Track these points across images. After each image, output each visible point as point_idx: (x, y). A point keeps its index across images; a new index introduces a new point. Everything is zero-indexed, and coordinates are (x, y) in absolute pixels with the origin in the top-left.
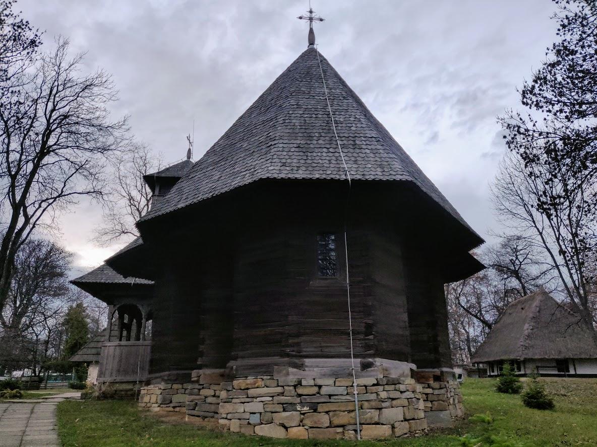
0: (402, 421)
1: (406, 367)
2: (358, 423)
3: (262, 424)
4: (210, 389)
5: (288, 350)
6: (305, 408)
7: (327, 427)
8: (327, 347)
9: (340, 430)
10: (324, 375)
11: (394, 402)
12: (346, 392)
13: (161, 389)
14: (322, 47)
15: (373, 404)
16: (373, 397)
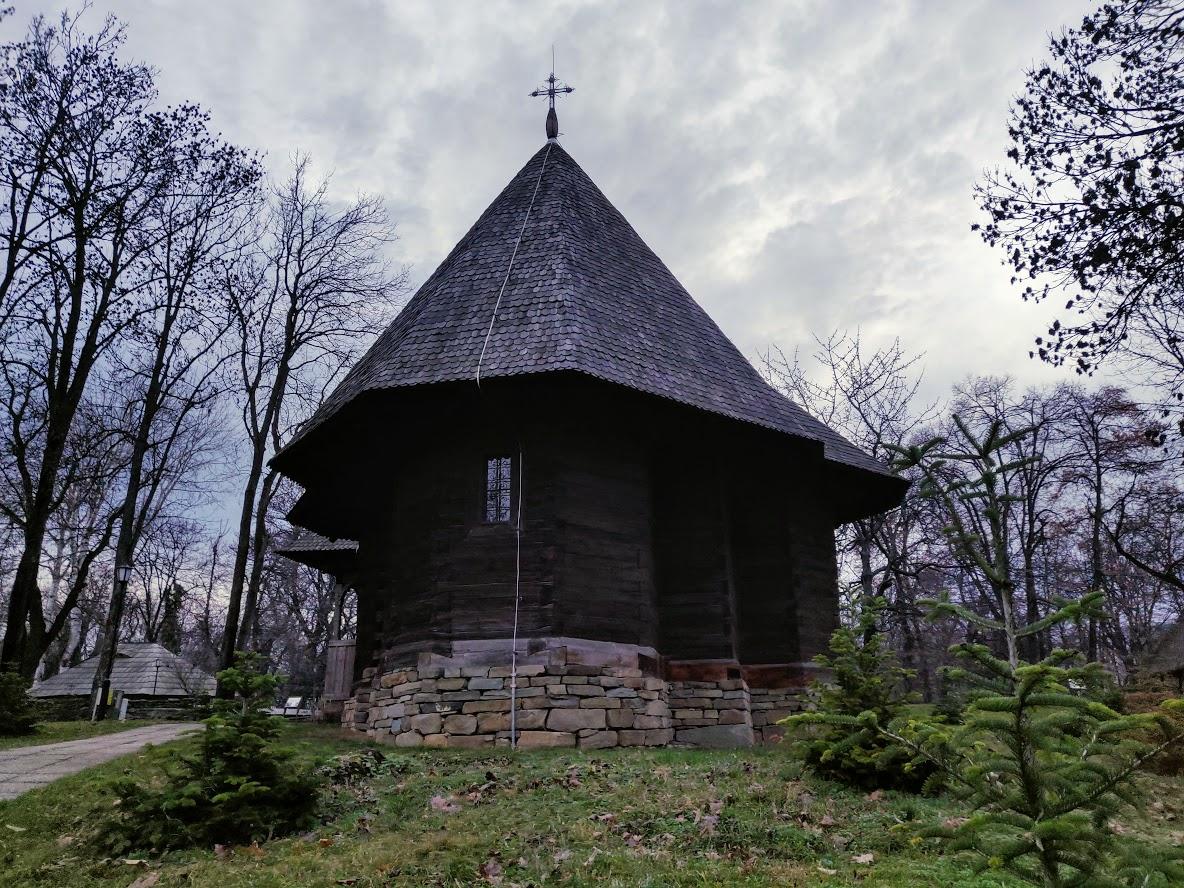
2: (513, 728)
5: (435, 629)
6: (446, 709)
7: (473, 734)
8: (486, 623)
9: (490, 738)
10: (477, 663)
11: (583, 701)
12: (501, 687)
14: (561, 141)
15: (539, 701)
16: (540, 691)
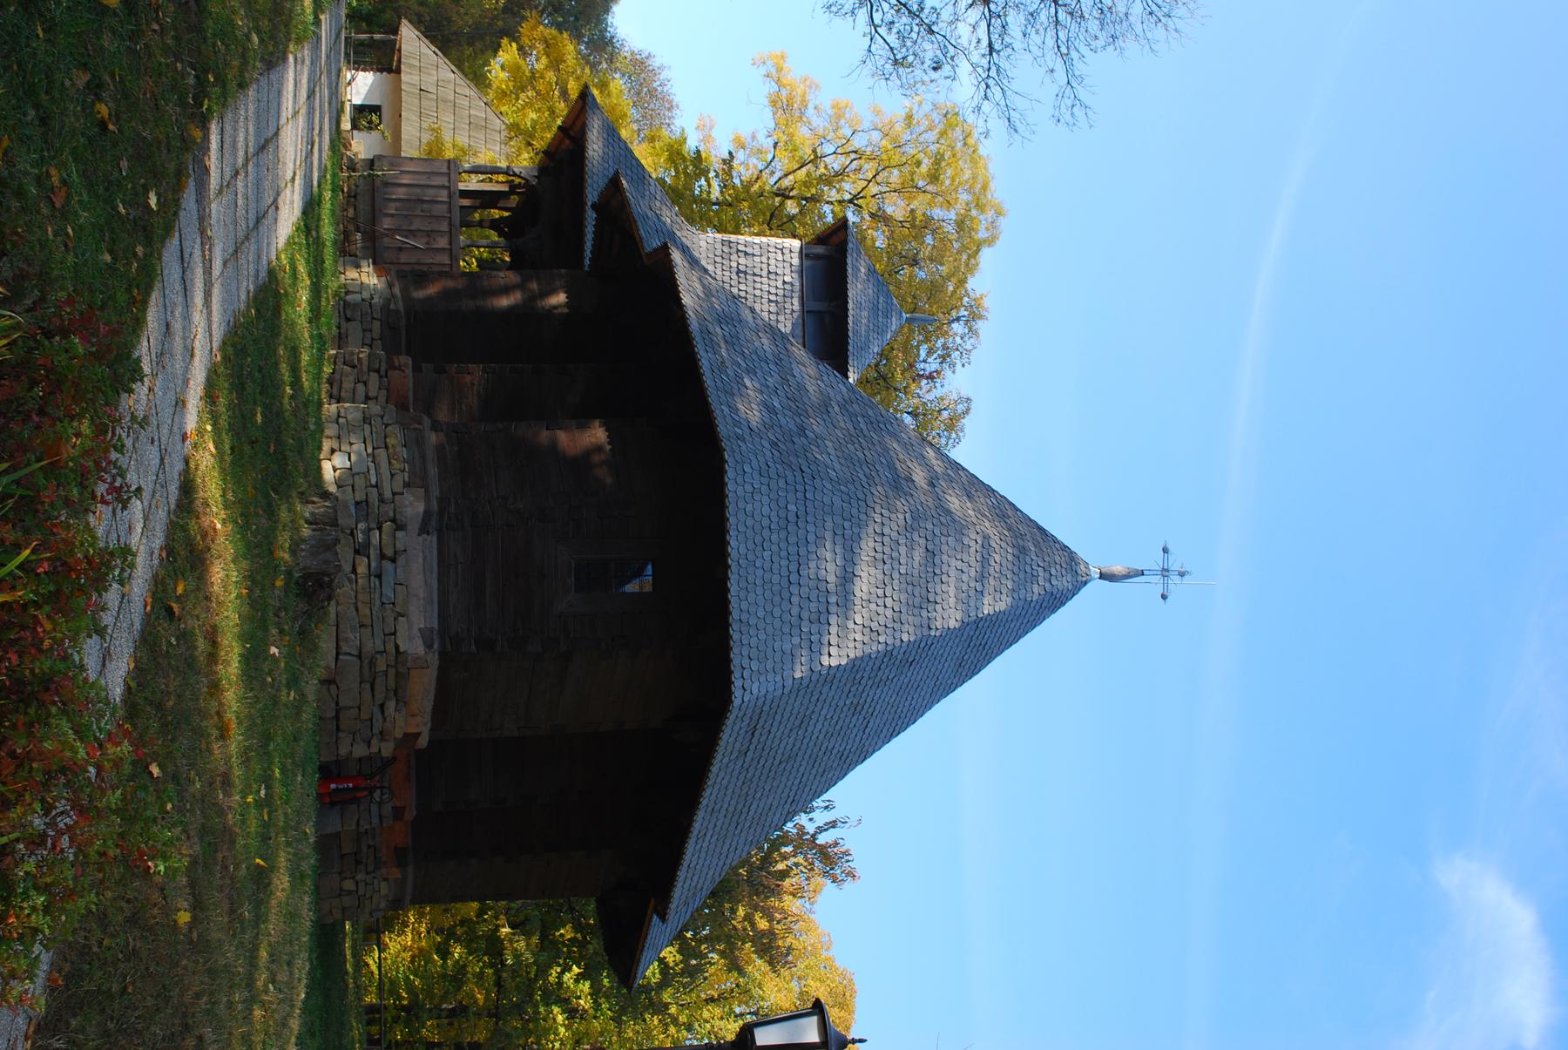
0: (337, 703)
1: (422, 726)
4: (380, 389)
11: (368, 687)
12: (384, 600)
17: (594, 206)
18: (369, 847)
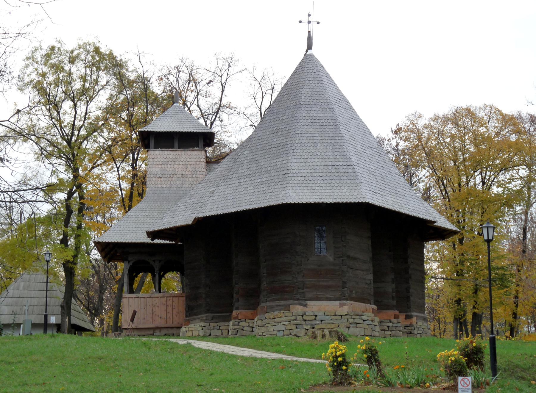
0: (363, 336)
3: (284, 336)
11: (358, 325)
13: (202, 326)
17: (152, 240)
18: (405, 329)
